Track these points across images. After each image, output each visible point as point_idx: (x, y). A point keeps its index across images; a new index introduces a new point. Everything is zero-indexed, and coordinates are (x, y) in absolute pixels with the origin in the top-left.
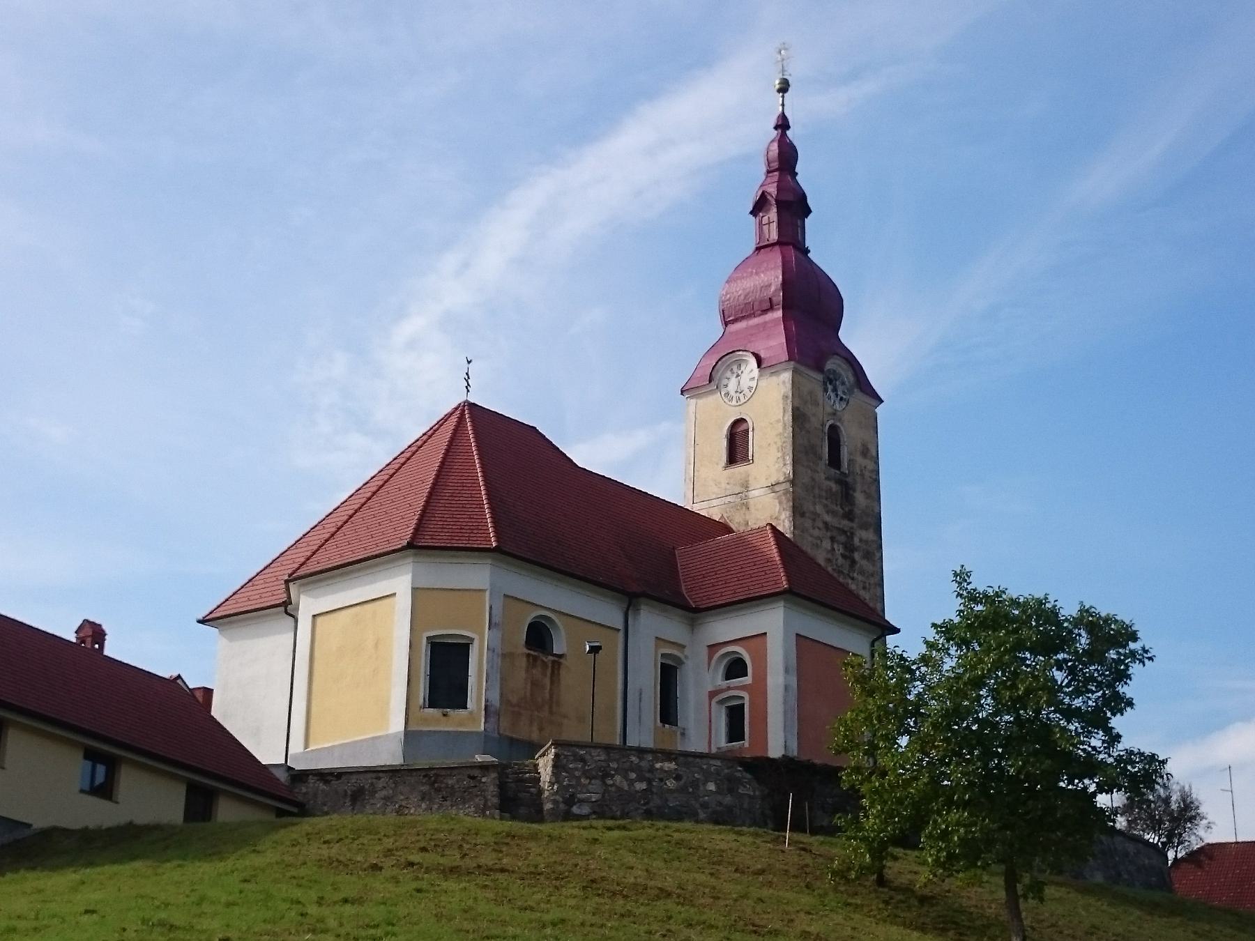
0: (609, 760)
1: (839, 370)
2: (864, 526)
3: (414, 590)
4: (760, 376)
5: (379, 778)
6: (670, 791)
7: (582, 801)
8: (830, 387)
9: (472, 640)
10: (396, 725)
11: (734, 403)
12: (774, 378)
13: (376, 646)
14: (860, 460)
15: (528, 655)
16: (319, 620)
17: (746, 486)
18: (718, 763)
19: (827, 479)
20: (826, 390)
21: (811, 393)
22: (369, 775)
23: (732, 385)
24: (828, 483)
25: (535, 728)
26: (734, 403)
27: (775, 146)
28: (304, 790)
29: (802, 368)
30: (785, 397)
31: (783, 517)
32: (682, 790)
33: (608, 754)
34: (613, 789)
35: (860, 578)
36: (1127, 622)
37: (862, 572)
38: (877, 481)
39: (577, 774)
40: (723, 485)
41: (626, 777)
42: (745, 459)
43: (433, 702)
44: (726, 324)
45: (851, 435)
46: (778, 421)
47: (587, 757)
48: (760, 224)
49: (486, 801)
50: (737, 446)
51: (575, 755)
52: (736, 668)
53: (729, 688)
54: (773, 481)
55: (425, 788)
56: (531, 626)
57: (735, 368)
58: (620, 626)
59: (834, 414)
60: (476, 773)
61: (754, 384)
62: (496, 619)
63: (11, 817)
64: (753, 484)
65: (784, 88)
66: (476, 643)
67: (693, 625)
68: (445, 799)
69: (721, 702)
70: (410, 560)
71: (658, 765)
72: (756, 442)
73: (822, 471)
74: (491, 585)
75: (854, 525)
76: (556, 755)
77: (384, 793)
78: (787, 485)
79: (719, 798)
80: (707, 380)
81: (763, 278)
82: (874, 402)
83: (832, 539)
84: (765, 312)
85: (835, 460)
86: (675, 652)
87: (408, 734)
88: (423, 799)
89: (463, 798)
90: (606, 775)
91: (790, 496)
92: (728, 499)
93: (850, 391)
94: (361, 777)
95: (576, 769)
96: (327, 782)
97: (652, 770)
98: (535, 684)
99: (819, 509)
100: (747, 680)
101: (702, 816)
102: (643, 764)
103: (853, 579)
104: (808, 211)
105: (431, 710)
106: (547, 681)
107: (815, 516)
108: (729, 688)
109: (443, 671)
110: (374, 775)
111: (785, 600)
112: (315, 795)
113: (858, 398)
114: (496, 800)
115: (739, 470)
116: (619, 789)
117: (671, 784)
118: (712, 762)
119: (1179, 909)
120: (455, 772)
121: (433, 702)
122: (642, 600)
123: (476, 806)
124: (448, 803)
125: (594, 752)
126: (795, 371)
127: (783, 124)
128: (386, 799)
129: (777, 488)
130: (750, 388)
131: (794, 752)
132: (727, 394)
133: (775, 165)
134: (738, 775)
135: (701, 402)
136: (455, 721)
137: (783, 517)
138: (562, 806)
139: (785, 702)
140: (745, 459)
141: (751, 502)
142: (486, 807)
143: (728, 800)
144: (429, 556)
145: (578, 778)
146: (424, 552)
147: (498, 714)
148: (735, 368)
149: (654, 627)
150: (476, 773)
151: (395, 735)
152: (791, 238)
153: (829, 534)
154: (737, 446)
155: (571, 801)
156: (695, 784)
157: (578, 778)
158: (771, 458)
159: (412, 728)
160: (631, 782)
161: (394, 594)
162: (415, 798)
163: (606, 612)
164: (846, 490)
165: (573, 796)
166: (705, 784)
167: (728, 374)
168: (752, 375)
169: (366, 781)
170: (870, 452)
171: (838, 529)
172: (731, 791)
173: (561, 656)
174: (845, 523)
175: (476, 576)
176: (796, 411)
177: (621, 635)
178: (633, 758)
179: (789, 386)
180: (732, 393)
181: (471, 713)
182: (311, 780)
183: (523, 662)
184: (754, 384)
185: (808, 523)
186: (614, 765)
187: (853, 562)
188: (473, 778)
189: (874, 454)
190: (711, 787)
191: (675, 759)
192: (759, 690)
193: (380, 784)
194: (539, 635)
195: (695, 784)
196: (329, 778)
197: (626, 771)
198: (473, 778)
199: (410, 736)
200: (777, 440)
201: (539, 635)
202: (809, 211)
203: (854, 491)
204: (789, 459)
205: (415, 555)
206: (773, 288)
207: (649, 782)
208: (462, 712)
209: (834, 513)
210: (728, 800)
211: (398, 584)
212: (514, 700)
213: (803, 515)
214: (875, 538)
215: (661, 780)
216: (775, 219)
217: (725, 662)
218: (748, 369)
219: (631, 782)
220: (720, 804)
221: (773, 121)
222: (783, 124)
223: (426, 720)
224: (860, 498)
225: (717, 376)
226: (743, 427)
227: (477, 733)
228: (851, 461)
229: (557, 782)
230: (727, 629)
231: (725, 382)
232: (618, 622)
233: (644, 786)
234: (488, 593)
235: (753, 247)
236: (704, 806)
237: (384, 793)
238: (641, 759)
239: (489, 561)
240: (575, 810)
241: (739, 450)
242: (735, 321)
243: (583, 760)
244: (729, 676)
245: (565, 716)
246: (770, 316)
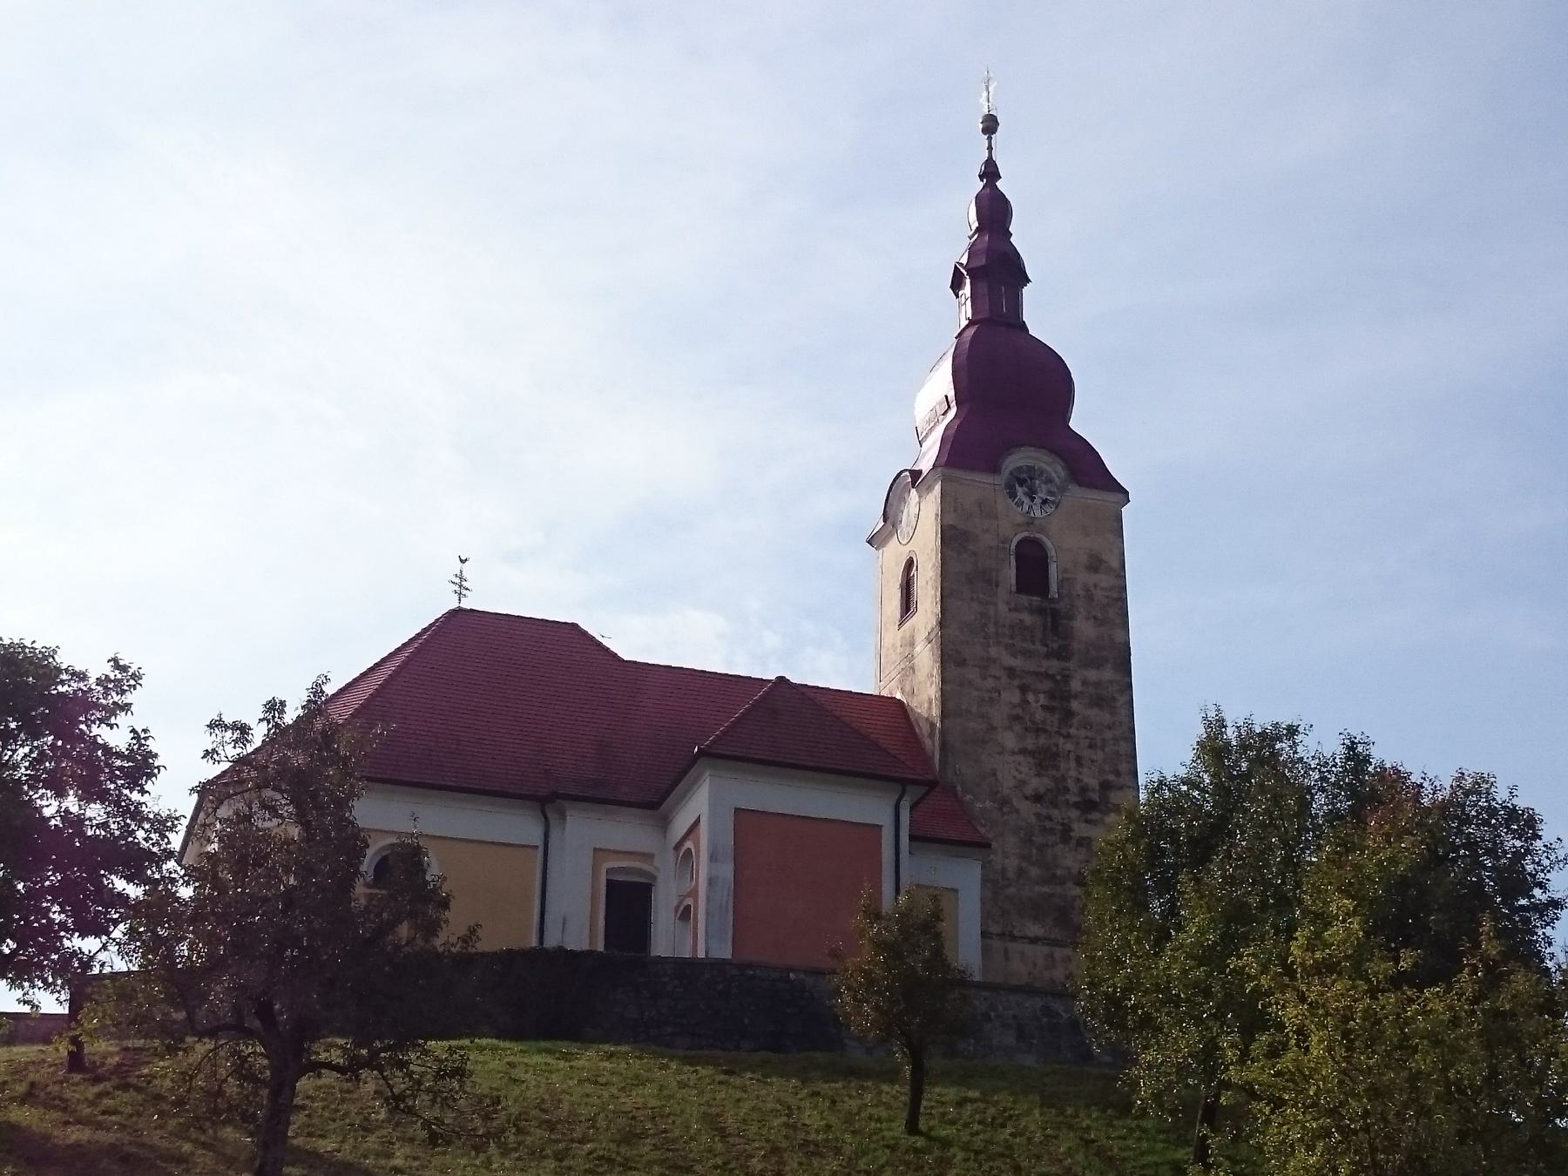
1: (1030, 462)
2: (1097, 664)
8: (1020, 491)
20: (1013, 495)
24: (1015, 615)
29: (958, 473)
35: (1083, 733)
36: (778, 568)
37: (1087, 724)
45: (1065, 547)
58: (539, 842)
59: (1030, 522)
65: (990, 125)
73: (1005, 602)
83: (1024, 689)
86: (646, 867)
91: (936, 644)
93: (1063, 490)
103: (1068, 736)
107: (986, 663)
113: (1078, 496)
153: (1016, 682)
163: (520, 827)
164: (1055, 622)
171: (1036, 674)
174: (1054, 665)
185: (972, 674)
187: (1069, 714)
189: (1115, 564)
203: (1071, 618)
209: (1028, 654)
213: (962, 663)
221: (978, 167)
222: (990, 172)
224: (1084, 628)
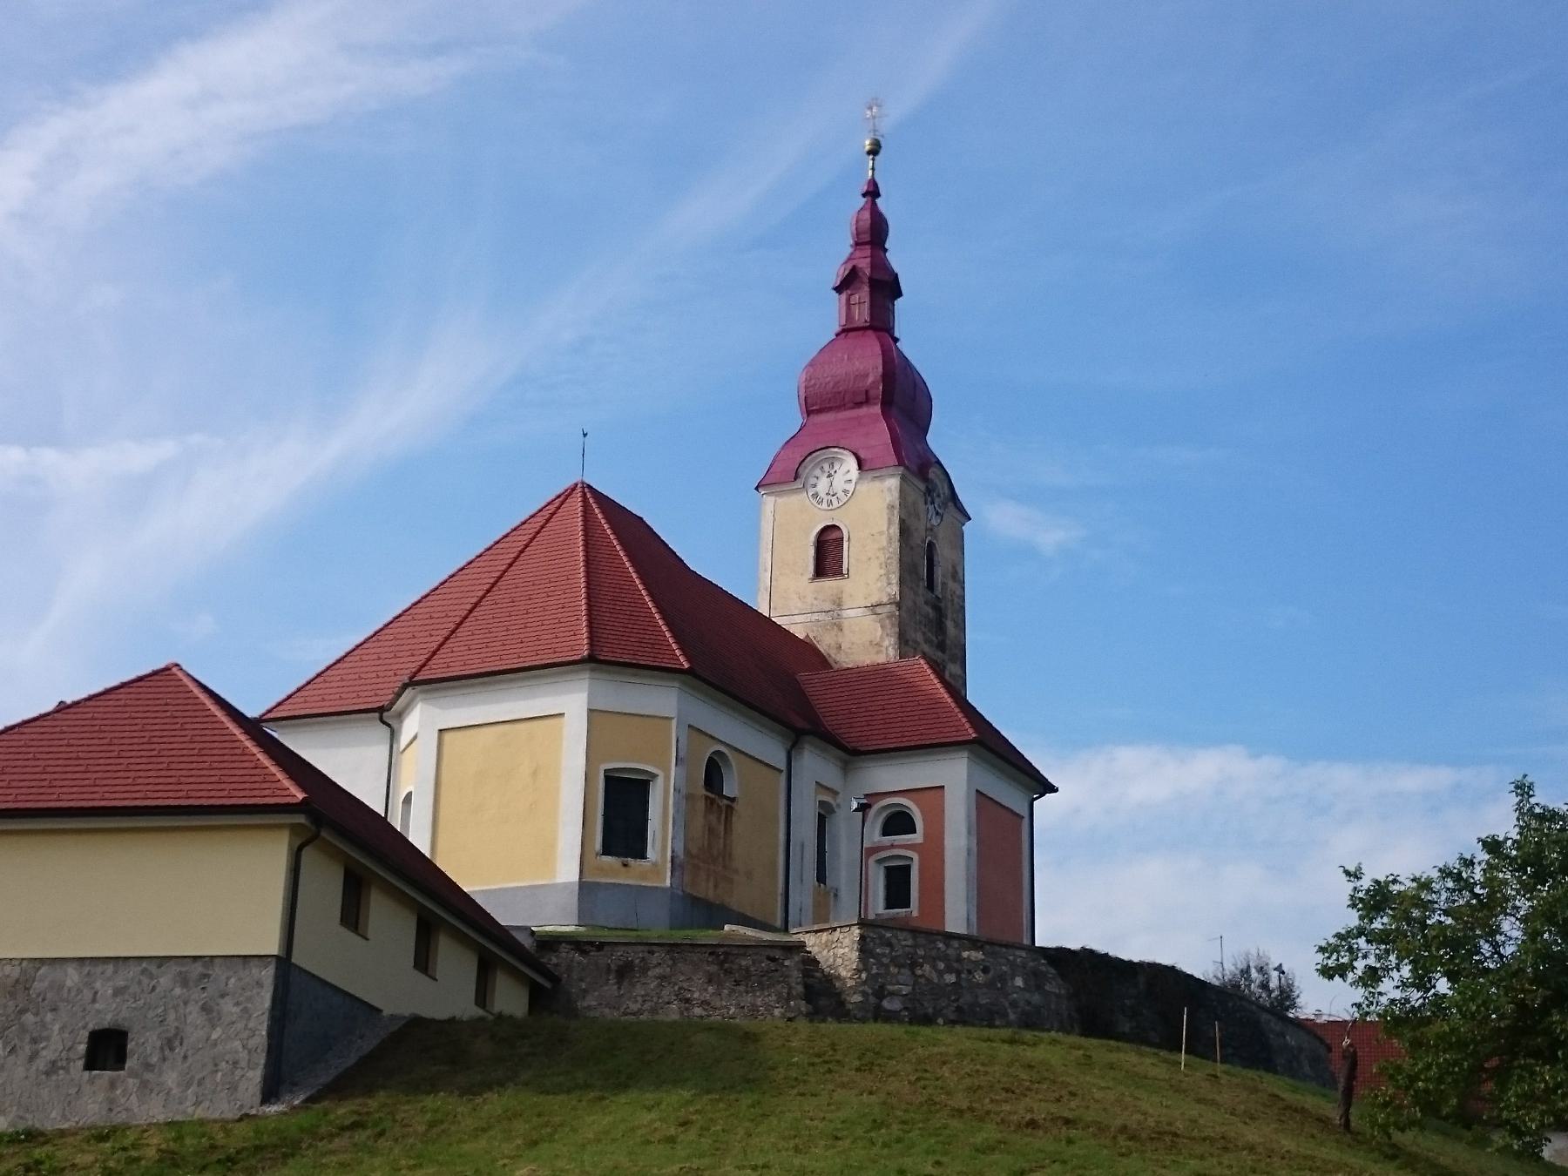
0: (915, 946)
2: (953, 660)
3: (590, 711)
4: (860, 479)
5: (652, 953)
6: (978, 985)
7: (892, 994)
9: (655, 776)
10: (567, 871)
11: (825, 505)
12: (877, 484)
13: (535, 774)
14: (951, 584)
15: (707, 798)
16: (447, 737)
17: (838, 603)
18: (1024, 954)
19: (926, 603)
21: (914, 503)
22: (640, 948)
23: (823, 485)
25: (711, 885)
26: (825, 505)
27: (867, 215)
28: (554, 960)
30: (891, 507)
31: (886, 643)
32: (990, 985)
33: (914, 938)
34: (922, 980)
38: (963, 608)
39: (885, 961)
40: (810, 599)
41: (934, 967)
42: (838, 572)
43: (607, 850)
44: (809, 413)
45: (943, 552)
46: (881, 533)
47: (894, 941)
48: (848, 300)
49: (790, 988)
50: (828, 554)
51: (881, 937)
52: (899, 823)
53: (892, 846)
54: (874, 600)
55: (713, 968)
56: (710, 759)
57: (826, 466)
60: (777, 954)
61: (850, 487)
62: (681, 754)
63: (329, 980)
64: (847, 603)
65: (875, 151)
66: (660, 781)
67: (846, 768)
68: (737, 983)
69: (879, 861)
70: (587, 675)
71: (965, 954)
72: (851, 555)
74: (679, 710)
75: (946, 657)
76: (862, 937)
77: (658, 971)
78: (893, 608)
79: (1027, 995)
80: (786, 473)
81: (858, 365)
82: (960, 517)
84: (859, 405)
85: (931, 585)
87: (583, 885)
88: (710, 982)
89: (760, 983)
90: (913, 965)
92: (815, 617)
94: (629, 949)
95: (884, 955)
96: (584, 953)
97: (959, 959)
98: (711, 831)
99: (920, 637)
100: (917, 838)
101: (1012, 1017)
102: (950, 951)
104: (898, 293)
105: (605, 858)
106: (722, 828)
108: (892, 846)
109: (620, 810)
110: (646, 948)
111: (971, 751)
112: (569, 969)
114: (800, 989)
115: (829, 584)
116: (929, 981)
117: (979, 977)
118: (1018, 953)
119: (630, 1060)
120: (750, 952)
121: (607, 850)
122: (808, 738)
123: (779, 995)
124: (742, 988)
125: (901, 935)
126: (903, 478)
127: (873, 192)
128: (662, 978)
129: (879, 610)
130: (845, 491)
131: (974, 932)
132: (816, 495)
133: (867, 238)
134: (1043, 968)
135: (779, 500)
136: (632, 874)
137: (886, 643)
138: (872, 999)
139: (968, 869)
140: (838, 572)
141: (846, 624)
142: (789, 997)
143: (1036, 998)
144: (609, 672)
145: (887, 966)
146: (604, 667)
147: (682, 866)
148: (826, 466)
149: (814, 766)
150: (777, 954)
151: (566, 886)
152: (881, 325)
154: (828, 554)
155: (881, 993)
156: (1002, 978)
157: (887, 966)
158: (872, 573)
159: (588, 879)
160: (941, 974)
161: (562, 715)
162: (699, 978)
163: (770, 748)
165: (882, 987)
166: (1013, 979)
167: (818, 472)
168: (848, 477)
169: (635, 955)
170: (957, 576)
172: (1039, 988)
173: (733, 800)
175: (662, 700)
176: (902, 522)
177: (783, 777)
178: (941, 945)
179: (896, 494)
180: (822, 495)
181: (655, 864)
182: (564, 948)
183: (701, 805)
184: (850, 487)
186: (921, 952)
188: (773, 960)
190: (1019, 982)
191: (981, 948)
192: (934, 850)
193: (655, 959)
194: (713, 774)
195: (1002, 978)
196: (588, 948)
197: (934, 959)
198: (773, 960)
199: (586, 888)
200: (880, 554)
201: (713, 774)
202: (900, 294)
204: (895, 579)
205: (592, 670)
206: (870, 379)
207: (958, 973)
208: (639, 862)
210: (1036, 998)
211: (570, 704)
212: (694, 851)
213: (906, 643)
214: (959, 672)
215: (969, 972)
216: (867, 299)
217: (884, 815)
218: (845, 468)
219: (941, 974)
220: (1029, 1003)
222: (873, 192)
223: (601, 870)
224: (949, 624)
225: (804, 472)
226: (834, 535)
227: (664, 890)
228: (944, 584)
229: (866, 969)
230: (893, 777)
231: (812, 481)
232: (779, 759)
233: (950, 978)
234: (674, 722)
235: (837, 329)
236: (1014, 1004)
237: (658, 971)
238: (947, 946)
239: (677, 684)
240: (886, 1004)
241: (829, 561)
242: (819, 411)
243: (890, 945)
244: (886, 831)
245: (736, 871)
246: (864, 410)
